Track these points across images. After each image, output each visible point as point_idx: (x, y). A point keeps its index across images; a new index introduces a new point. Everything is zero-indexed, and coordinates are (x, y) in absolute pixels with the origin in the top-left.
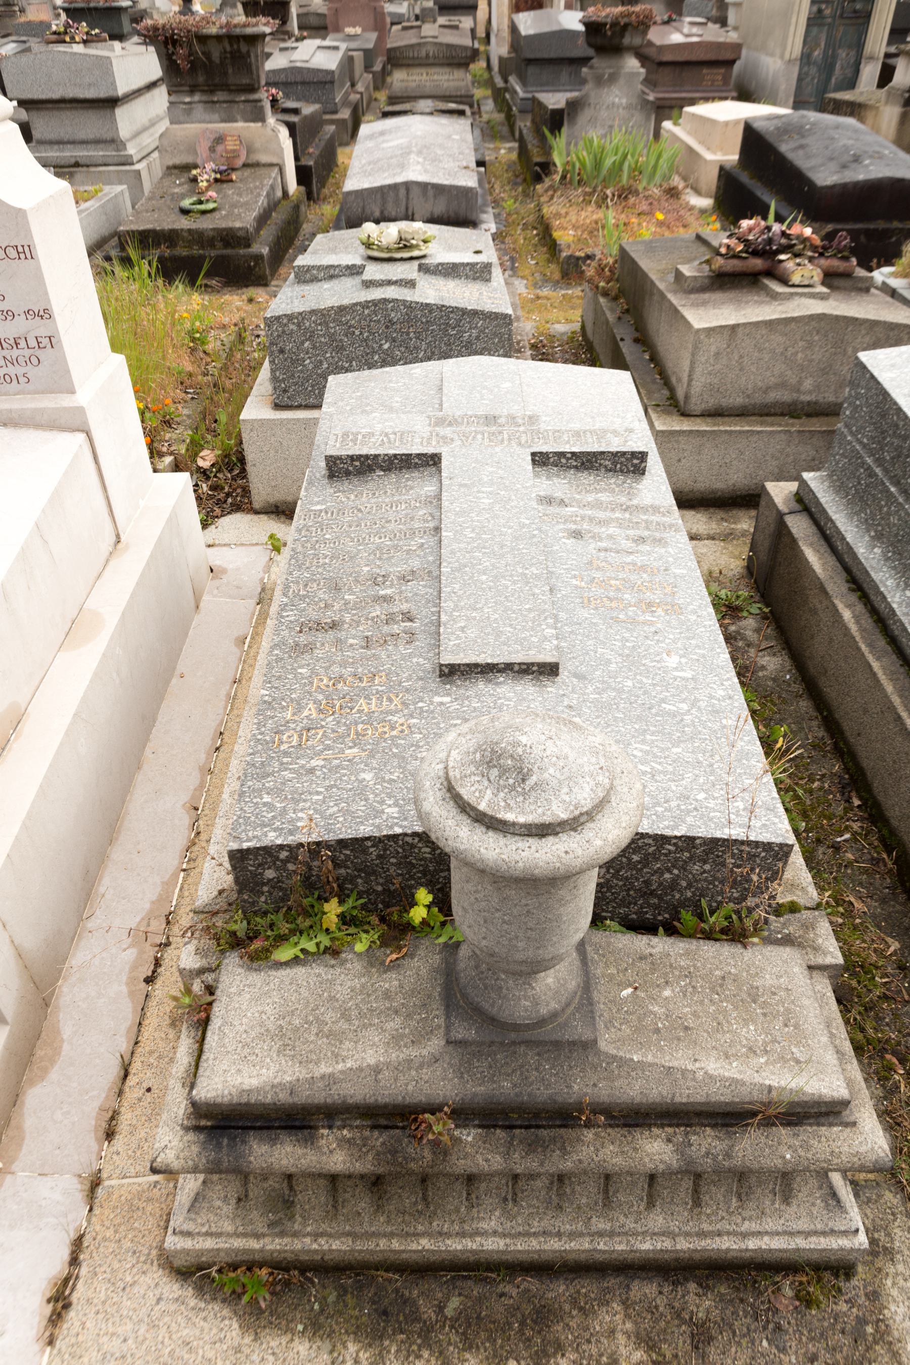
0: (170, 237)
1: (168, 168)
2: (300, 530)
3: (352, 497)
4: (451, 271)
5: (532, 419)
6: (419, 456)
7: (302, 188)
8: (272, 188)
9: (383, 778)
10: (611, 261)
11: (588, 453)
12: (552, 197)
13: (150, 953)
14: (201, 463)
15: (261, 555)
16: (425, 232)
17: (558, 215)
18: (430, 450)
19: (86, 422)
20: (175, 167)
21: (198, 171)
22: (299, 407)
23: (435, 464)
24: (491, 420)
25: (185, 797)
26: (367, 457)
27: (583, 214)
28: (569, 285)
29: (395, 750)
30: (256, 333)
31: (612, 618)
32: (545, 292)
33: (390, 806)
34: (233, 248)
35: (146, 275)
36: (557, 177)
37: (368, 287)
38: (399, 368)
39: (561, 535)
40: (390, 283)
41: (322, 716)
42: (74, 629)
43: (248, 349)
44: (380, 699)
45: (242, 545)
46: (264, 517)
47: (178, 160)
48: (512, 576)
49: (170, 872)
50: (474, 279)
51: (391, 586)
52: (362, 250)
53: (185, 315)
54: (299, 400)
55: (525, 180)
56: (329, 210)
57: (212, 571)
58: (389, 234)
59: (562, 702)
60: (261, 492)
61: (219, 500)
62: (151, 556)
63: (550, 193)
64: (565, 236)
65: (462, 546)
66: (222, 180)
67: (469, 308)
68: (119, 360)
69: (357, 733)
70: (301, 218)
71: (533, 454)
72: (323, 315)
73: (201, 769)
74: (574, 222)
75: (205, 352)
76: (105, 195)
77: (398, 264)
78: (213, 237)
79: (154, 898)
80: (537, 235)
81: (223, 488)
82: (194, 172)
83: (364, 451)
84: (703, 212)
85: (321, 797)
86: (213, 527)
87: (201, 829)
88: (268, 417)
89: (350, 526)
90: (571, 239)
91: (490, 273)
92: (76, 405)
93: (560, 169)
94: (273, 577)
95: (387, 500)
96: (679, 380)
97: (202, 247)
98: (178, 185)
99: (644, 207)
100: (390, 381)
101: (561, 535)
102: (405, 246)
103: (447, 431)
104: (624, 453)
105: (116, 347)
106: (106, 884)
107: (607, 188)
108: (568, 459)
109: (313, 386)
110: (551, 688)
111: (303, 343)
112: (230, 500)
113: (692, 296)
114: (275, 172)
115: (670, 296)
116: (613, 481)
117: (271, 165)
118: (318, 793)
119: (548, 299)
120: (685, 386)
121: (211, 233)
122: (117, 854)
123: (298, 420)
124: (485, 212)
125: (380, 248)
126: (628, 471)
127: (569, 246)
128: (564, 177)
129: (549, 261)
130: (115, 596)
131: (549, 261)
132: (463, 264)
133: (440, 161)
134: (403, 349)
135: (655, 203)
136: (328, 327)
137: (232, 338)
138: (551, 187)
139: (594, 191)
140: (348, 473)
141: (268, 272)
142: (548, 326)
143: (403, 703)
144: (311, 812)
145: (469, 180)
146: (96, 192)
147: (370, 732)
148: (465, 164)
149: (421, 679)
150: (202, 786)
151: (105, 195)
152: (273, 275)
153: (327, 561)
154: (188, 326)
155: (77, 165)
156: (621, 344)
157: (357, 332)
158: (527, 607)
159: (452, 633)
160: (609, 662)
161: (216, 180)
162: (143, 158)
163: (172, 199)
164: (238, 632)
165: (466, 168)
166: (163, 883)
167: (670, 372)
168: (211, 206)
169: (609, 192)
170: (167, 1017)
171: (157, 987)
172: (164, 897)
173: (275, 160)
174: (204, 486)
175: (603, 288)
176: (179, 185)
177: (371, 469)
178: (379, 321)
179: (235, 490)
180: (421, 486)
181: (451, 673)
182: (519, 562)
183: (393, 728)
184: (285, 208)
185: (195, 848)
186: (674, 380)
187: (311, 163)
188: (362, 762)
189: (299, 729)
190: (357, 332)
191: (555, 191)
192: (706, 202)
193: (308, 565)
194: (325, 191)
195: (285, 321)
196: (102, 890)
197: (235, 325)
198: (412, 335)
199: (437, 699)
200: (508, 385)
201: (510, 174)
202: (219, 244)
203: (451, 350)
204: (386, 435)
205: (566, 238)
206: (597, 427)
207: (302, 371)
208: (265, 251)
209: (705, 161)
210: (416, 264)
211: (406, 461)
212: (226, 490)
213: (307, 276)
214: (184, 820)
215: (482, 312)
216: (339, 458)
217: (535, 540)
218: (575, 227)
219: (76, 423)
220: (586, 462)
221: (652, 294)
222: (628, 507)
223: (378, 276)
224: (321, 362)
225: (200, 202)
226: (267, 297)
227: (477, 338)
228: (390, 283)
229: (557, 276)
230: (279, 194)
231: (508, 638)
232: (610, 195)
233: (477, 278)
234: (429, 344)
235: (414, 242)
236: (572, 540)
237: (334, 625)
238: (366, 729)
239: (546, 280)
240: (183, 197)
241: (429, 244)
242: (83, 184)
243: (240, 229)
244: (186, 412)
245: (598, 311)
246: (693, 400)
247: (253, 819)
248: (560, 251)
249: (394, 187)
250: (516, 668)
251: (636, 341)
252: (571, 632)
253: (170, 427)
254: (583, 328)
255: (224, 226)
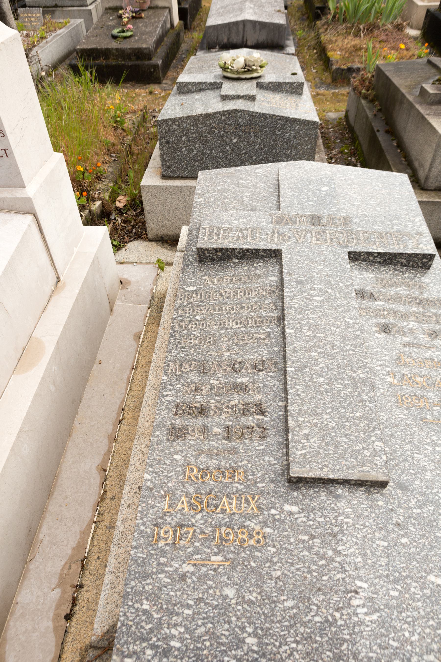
0: (105, 53)
1: (106, 9)
2: (178, 309)
3: (216, 281)
4: (276, 87)
5: (347, 220)
6: (265, 250)
7: (182, 22)
8: (165, 22)
9: (243, 597)
10: (369, 75)
11: (390, 254)
12: (326, 30)
13: (70, 592)
14: (118, 204)
15: (151, 271)
16: (262, 61)
17: (331, 42)
18: (273, 246)
19: (33, 208)
20: (110, 8)
21: (123, 11)
22: (178, 178)
23: (276, 256)
24: (316, 220)
25: (98, 461)
26: (227, 250)
27: (346, 41)
28: (336, 87)
29: (253, 564)
30: (153, 114)
31: (422, 419)
32: (322, 91)
33: (250, 635)
34: (142, 60)
35: (89, 80)
36: (330, 17)
37: (224, 100)
38: (248, 168)
39: (374, 329)
40: (239, 97)
41: (192, 512)
42: (24, 356)
43: (148, 125)
44: (239, 499)
45: (141, 263)
46: (154, 244)
47: (111, 5)
48: (343, 379)
49: (86, 523)
50: (292, 93)
51: (247, 373)
52: (219, 72)
53: (111, 107)
54: (178, 174)
55: (308, 18)
56: (196, 35)
57: (121, 283)
58: (238, 62)
59: (391, 518)
60: (153, 228)
61: (128, 231)
62: (79, 293)
63: (326, 27)
64: (335, 55)
65: (302, 344)
66: (136, 17)
67: (291, 117)
68: (60, 156)
69: (221, 538)
70: (181, 41)
71: (350, 253)
72: (195, 120)
73: (109, 437)
74: (339, 46)
75: (123, 129)
76: (71, 25)
77: (244, 82)
78: (130, 54)
79: (75, 546)
80: (316, 53)
81: (130, 222)
82: (120, 12)
83: (225, 245)
84: (415, 38)
85: (190, 612)
86: (124, 249)
87: (107, 488)
88: (158, 184)
89: (214, 309)
90: (338, 57)
91: (302, 89)
92: (25, 196)
93: (332, 12)
94: (159, 288)
95: (241, 287)
96: (422, 165)
97: (124, 60)
98: (111, 21)
99: (383, 37)
100: (241, 179)
101: (374, 329)
102: (249, 70)
103: (284, 229)
104: (418, 255)
105: (56, 148)
106: (44, 533)
107: (361, 24)
108: (375, 257)
109: (186, 165)
110: (380, 500)
111: (181, 137)
112: (134, 231)
113: (434, 107)
114: (166, 12)
115: (417, 106)
116: (407, 275)
117: (165, 8)
118: (189, 607)
119: (324, 95)
120: (427, 170)
121: (129, 51)
122: (53, 507)
123: (177, 187)
124: (289, 39)
125: (232, 72)
126: (418, 267)
127: (337, 62)
128: (334, 17)
129: (324, 70)
130: (54, 326)
131: (324, 70)
132: (285, 83)
133: (264, 7)
134: (245, 143)
135: (390, 34)
136: (198, 128)
137: (139, 119)
138: (326, 23)
139: (353, 26)
140: (212, 260)
141: (161, 75)
142: (325, 113)
143: (259, 508)
144: (182, 630)
145: (281, 20)
146: (66, 23)
147: (231, 537)
148: (278, 9)
149: (273, 481)
150: (109, 452)
151: (71, 25)
152: (164, 77)
153: (197, 342)
154: (113, 113)
155: (56, 6)
156: (378, 134)
157: (216, 131)
158: (358, 414)
159: (299, 441)
160: (424, 469)
161: (133, 17)
162: (93, 2)
163: (108, 29)
164: (136, 330)
165: (279, 11)
166: (81, 532)
167: (413, 158)
168: (129, 34)
169: (361, 27)
170: (78, 654)
171: (73, 624)
172: (80, 546)
173: (167, 5)
174: (119, 220)
175: (364, 94)
176: (112, 20)
177: (229, 258)
178: (231, 124)
179: (138, 223)
180: (266, 274)
181: (297, 483)
182: (348, 364)
183: (251, 537)
184: (172, 34)
185: (103, 504)
186: (416, 164)
187: (187, 6)
188: (225, 574)
189: (173, 524)
190: (216, 131)
191: (328, 26)
192: (414, 33)
193: (183, 345)
194: (195, 23)
195: (170, 123)
196: (41, 536)
197: (141, 110)
198: (252, 134)
199: (287, 507)
200: (325, 188)
201: (300, 14)
202: (133, 58)
203: (276, 144)
204: (241, 231)
205: (335, 56)
206: (394, 230)
207: (180, 155)
208: (160, 62)
209: (417, 6)
210: (255, 82)
211: (255, 253)
212: (132, 223)
213: (185, 89)
214: (96, 479)
215: (299, 120)
216: (207, 250)
217: (359, 341)
218: (341, 50)
219: (27, 209)
220: (388, 260)
221: (402, 103)
222: (421, 301)
223: (231, 92)
224: (192, 150)
225: (123, 31)
226: (160, 91)
227: (295, 137)
228: (239, 97)
229: (329, 80)
230: (169, 26)
231: (345, 450)
232: (362, 29)
233: (294, 92)
234: (262, 140)
235: (254, 68)
236: (383, 334)
237: (202, 411)
238: (228, 534)
239: (323, 83)
240: (114, 27)
241: (264, 69)
242: (59, 18)
243: (146, 49)
244: (110, 169)
245: (359, 108)
246: (431, 180)
247: (133, 628)
248: (332, 65)
249: (236, 24)
250: (353, 482)
251: (387, 132)
252: (392, 435)
253: (101, 180)
254: (346, 116)
255: (136, 46)
